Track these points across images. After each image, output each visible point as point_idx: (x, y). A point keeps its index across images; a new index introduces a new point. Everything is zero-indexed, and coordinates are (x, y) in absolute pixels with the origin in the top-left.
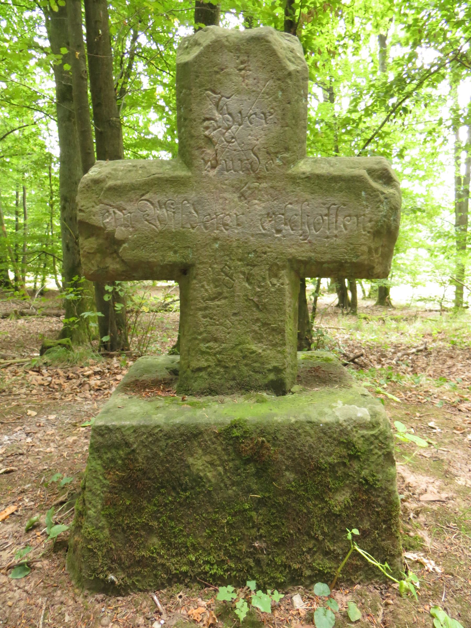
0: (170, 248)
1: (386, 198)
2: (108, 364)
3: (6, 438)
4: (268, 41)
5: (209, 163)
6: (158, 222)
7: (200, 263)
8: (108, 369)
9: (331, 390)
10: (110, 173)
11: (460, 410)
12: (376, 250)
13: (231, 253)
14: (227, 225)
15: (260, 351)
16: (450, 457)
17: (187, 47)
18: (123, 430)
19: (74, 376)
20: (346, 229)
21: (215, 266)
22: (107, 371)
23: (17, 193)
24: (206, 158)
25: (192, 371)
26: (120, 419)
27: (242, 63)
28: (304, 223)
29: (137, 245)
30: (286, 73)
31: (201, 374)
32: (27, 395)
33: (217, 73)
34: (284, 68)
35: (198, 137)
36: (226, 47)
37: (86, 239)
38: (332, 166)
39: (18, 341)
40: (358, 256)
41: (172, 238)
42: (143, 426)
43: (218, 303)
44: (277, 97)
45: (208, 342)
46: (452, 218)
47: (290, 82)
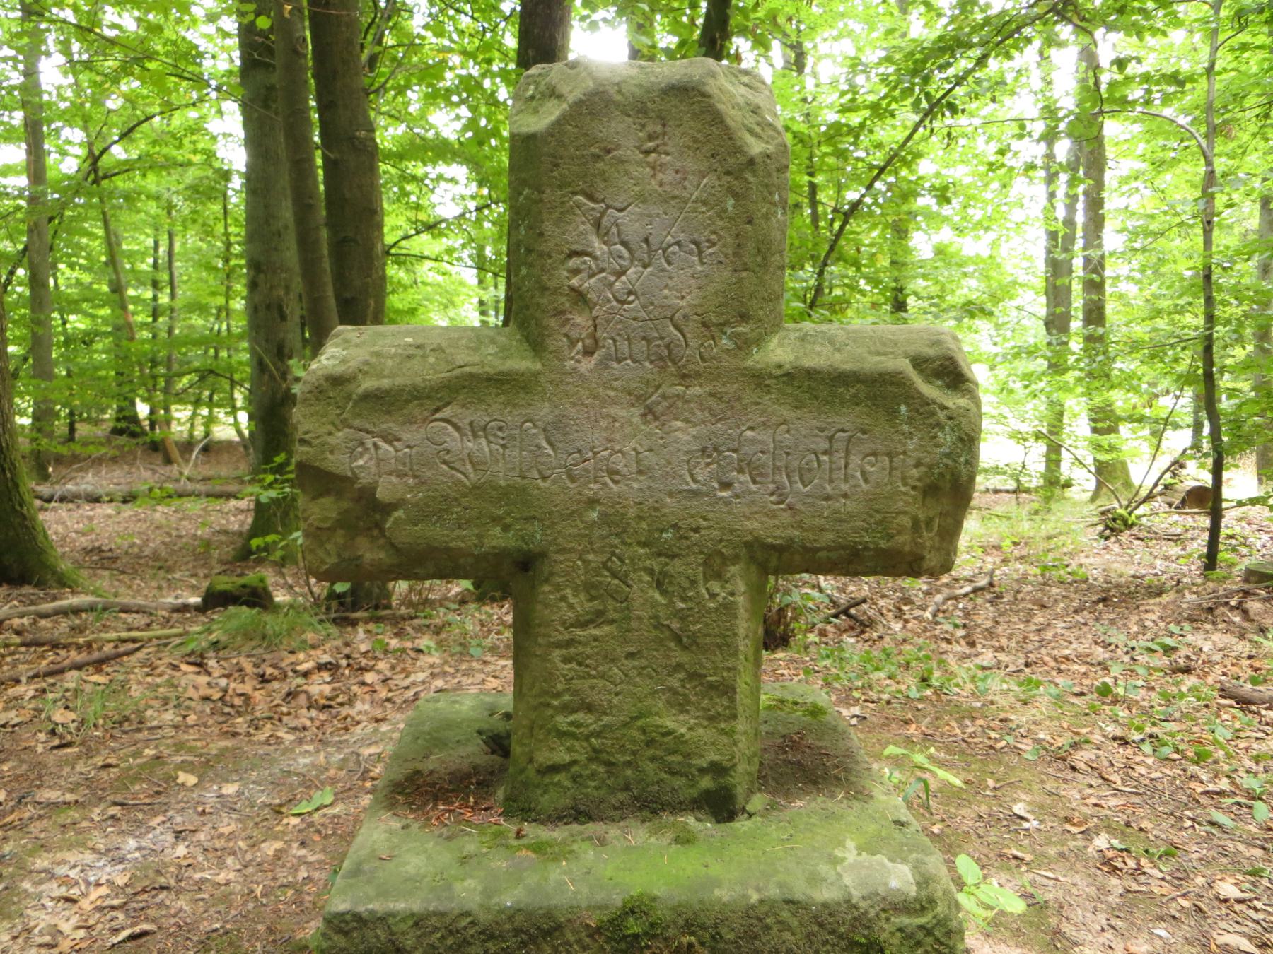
0: (496, 520)
1: (950, 418)
2: (347, 644)
3: (132, 843)
4: (704, 95)
5: (580, 345)
6: (469, 466)
7: (558, 552)
8: (348, 657)
9: (830, 804)
10: (366, 363)
11: (1073, 768)
12: (929, 523)
13: (625, 531)
14: (617, 472)
15: (683, 730)
16: (1060, 894)
17: (532, 98)
18: (391, 921)
19: (276, 672)
20: (866, 481)
21: (590, 557)
22: (344, 662)
23: (156, 243)
24: (574, 335)
25: (538, 771)
26: (383, 894)
27: (651, 137)
28: (778, 468)
29: (423, 513)
30: (743, 160)
31: (557, 778)
32: (176, 727)
33: (597, 158)
34: (738, 150)
35: (556, 291)
36: (617, 105)
37: (314, 499)
38: (839, 350)
39: (155, 556)
40: (890, 537)
41: (500, 500)
42: (435, 914)
43: (597, 632)
44: (725, 210)
45: (573, 711)
46: (1040, 306)
47: (751, 179)
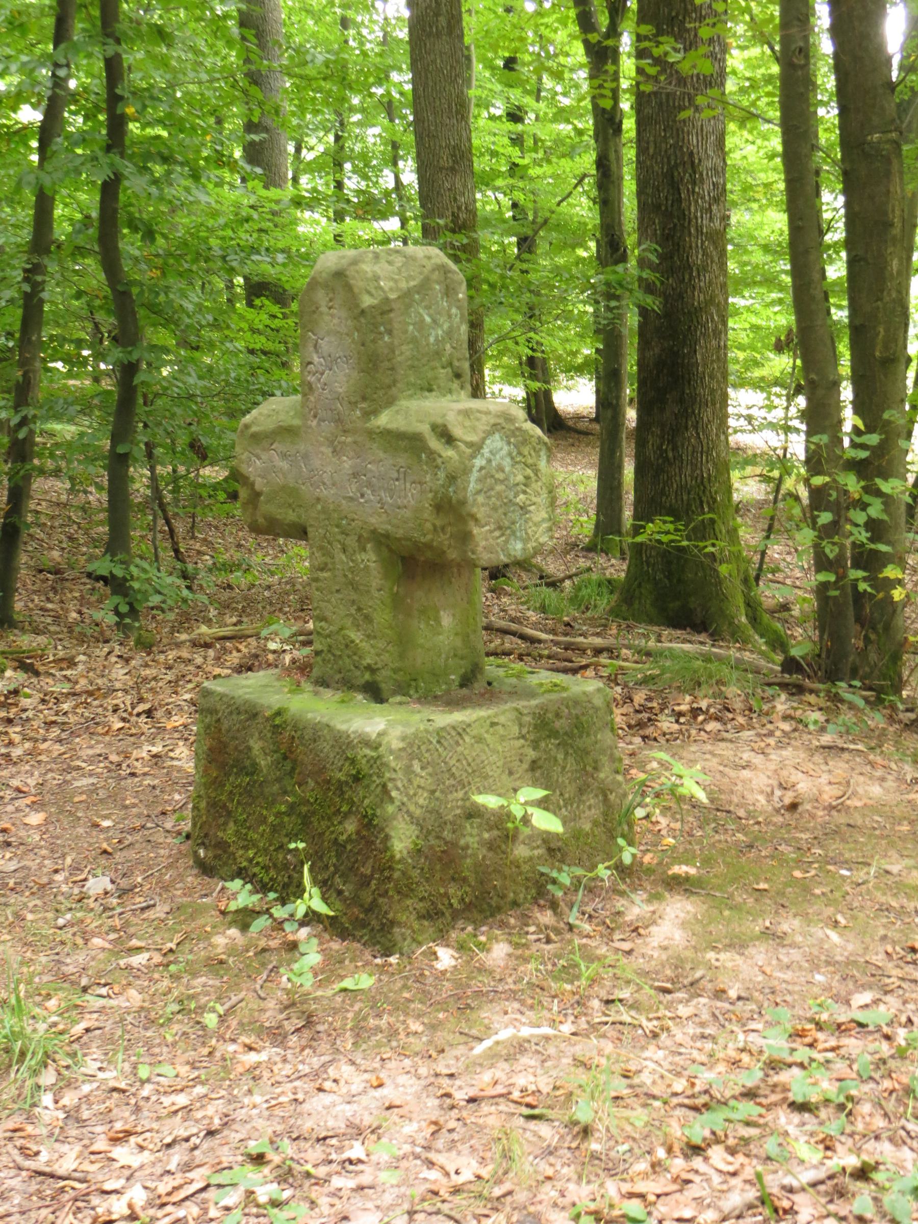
12: (443, 529)
